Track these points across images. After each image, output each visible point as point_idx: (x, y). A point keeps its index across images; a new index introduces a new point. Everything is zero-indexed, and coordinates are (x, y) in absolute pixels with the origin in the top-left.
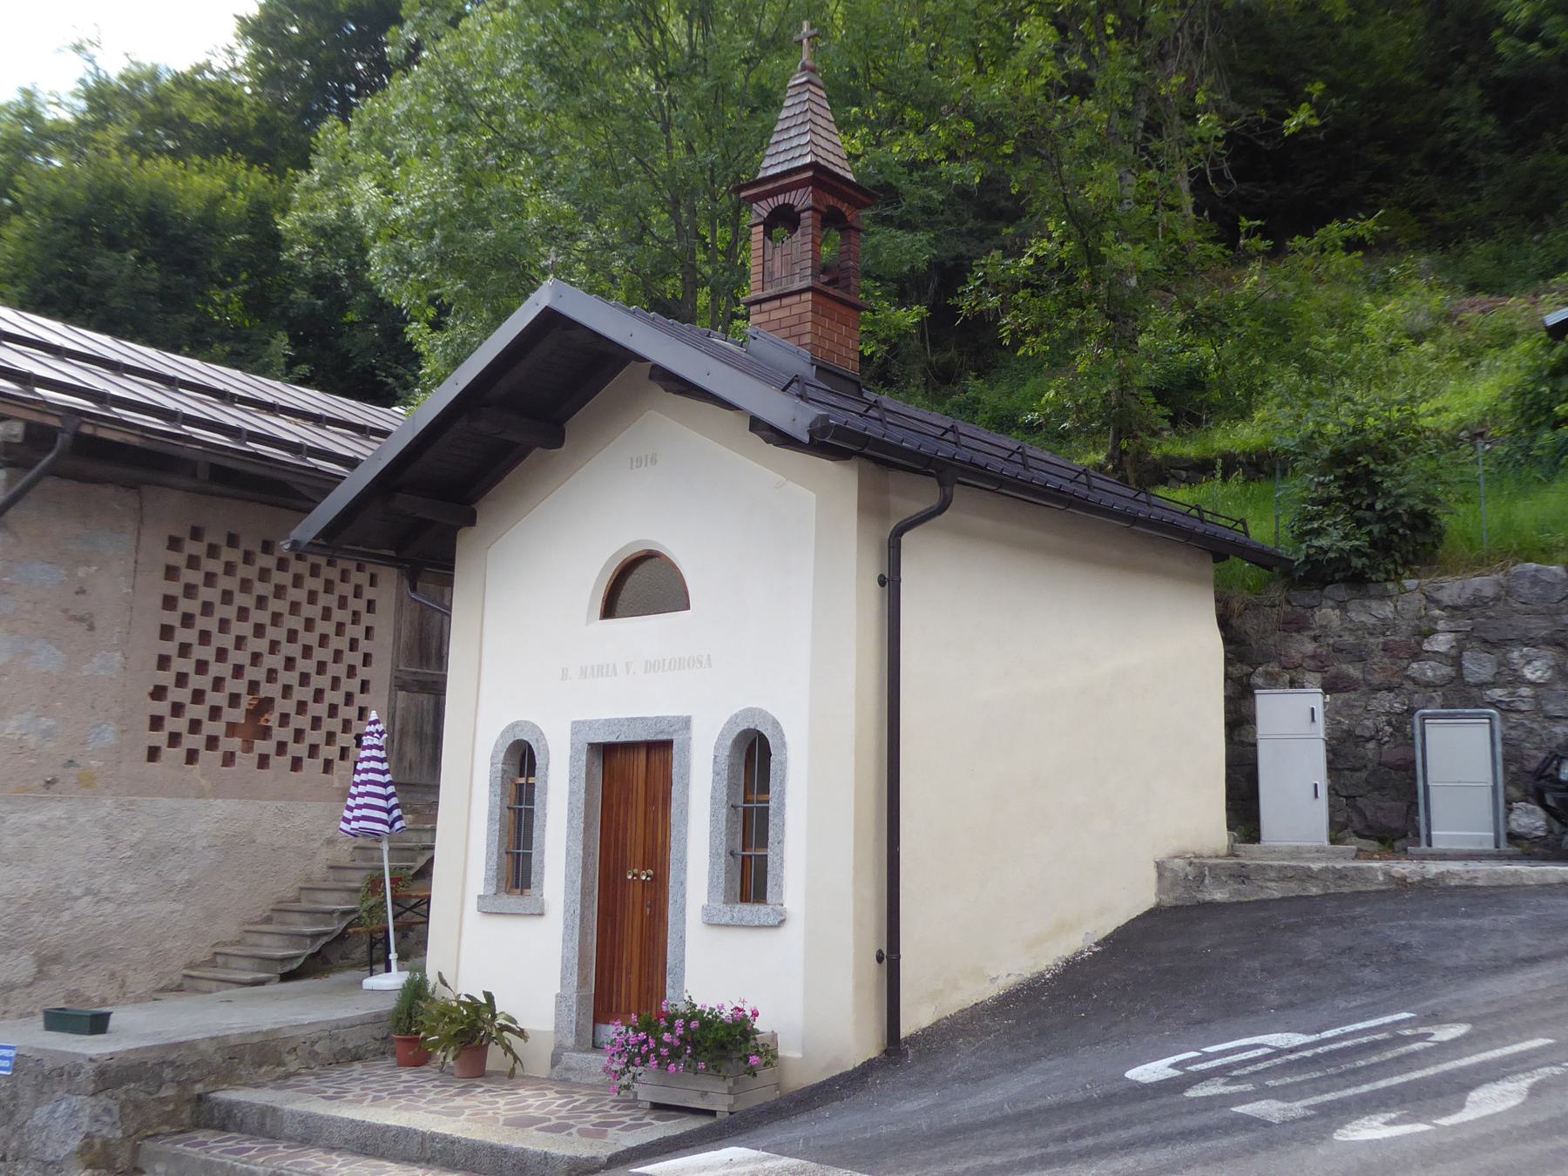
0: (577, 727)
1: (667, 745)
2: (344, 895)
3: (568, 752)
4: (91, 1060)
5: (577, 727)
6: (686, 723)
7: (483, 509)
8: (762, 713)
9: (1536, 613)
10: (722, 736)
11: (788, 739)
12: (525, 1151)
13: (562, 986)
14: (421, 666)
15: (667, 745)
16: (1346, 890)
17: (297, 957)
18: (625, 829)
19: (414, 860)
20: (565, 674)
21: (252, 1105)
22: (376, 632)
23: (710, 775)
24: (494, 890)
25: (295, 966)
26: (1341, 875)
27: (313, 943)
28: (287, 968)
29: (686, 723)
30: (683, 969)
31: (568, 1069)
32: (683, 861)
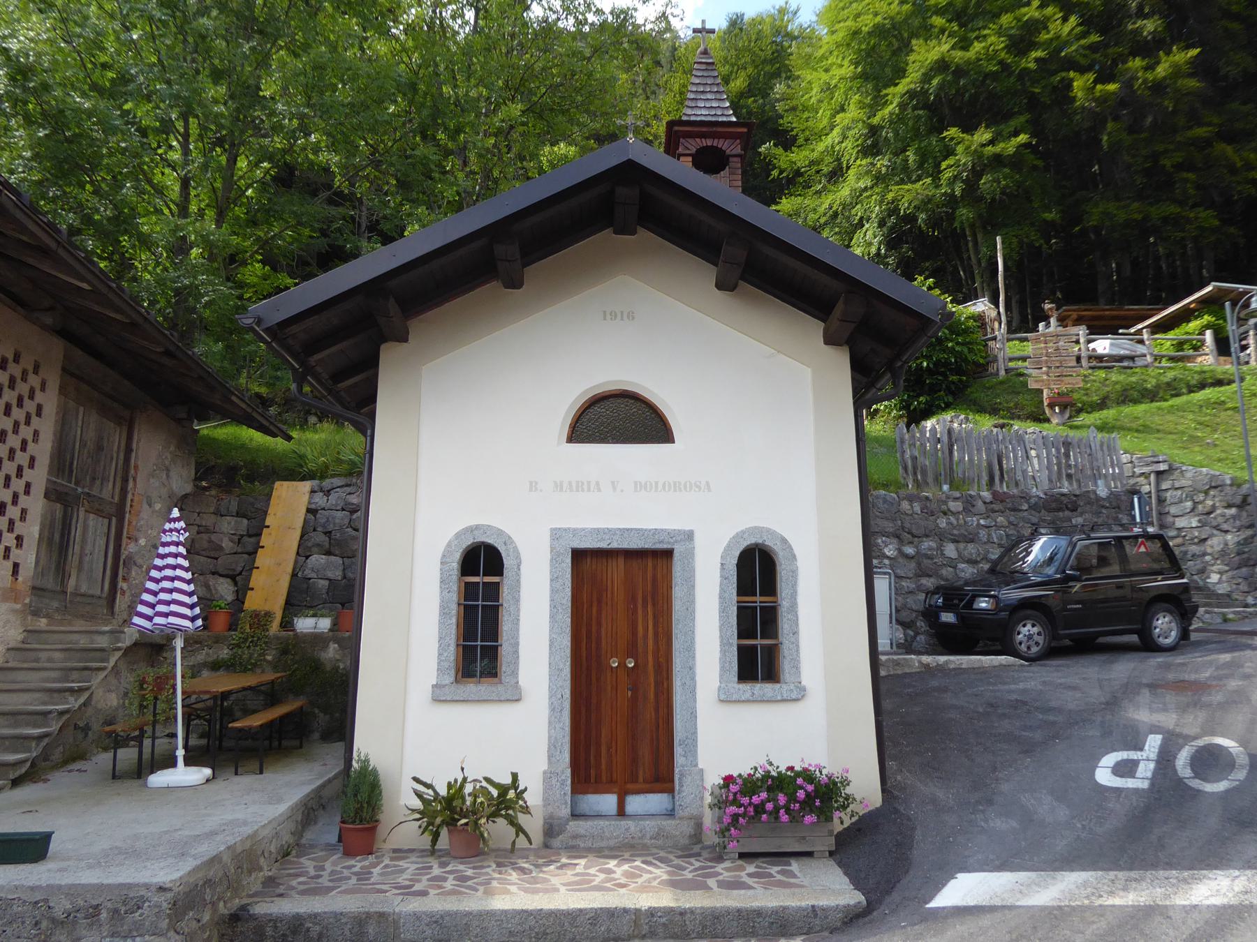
0: (556, 534)
1: (668, 554)
2: (37, 695)
3: (546, 556)
4: (162, 889)
5: (556, 534)
6: (690, 536)
7: (416, 327)
8: (508, 540)
9: (887, 519)
10: (728, 548)
11: (797, 551)
12: (785, 908)
13: (550, 762)
14: (57, 477)
15: (668, 554)
16: (900, 672)
17: (24, 761)
18: (599, 624)
19: (107, 660)
20: (533, 486)
21: (337, 916)
22: (42, 436)
23: (717, 579)
24: (452, 679)
25: (23, 770)
26: (897, 663)
27: (38, 745)
28: (17, 774)
29: (690, 536)
30: (695, 741)
31: (575, 837)
32: (690, 649)
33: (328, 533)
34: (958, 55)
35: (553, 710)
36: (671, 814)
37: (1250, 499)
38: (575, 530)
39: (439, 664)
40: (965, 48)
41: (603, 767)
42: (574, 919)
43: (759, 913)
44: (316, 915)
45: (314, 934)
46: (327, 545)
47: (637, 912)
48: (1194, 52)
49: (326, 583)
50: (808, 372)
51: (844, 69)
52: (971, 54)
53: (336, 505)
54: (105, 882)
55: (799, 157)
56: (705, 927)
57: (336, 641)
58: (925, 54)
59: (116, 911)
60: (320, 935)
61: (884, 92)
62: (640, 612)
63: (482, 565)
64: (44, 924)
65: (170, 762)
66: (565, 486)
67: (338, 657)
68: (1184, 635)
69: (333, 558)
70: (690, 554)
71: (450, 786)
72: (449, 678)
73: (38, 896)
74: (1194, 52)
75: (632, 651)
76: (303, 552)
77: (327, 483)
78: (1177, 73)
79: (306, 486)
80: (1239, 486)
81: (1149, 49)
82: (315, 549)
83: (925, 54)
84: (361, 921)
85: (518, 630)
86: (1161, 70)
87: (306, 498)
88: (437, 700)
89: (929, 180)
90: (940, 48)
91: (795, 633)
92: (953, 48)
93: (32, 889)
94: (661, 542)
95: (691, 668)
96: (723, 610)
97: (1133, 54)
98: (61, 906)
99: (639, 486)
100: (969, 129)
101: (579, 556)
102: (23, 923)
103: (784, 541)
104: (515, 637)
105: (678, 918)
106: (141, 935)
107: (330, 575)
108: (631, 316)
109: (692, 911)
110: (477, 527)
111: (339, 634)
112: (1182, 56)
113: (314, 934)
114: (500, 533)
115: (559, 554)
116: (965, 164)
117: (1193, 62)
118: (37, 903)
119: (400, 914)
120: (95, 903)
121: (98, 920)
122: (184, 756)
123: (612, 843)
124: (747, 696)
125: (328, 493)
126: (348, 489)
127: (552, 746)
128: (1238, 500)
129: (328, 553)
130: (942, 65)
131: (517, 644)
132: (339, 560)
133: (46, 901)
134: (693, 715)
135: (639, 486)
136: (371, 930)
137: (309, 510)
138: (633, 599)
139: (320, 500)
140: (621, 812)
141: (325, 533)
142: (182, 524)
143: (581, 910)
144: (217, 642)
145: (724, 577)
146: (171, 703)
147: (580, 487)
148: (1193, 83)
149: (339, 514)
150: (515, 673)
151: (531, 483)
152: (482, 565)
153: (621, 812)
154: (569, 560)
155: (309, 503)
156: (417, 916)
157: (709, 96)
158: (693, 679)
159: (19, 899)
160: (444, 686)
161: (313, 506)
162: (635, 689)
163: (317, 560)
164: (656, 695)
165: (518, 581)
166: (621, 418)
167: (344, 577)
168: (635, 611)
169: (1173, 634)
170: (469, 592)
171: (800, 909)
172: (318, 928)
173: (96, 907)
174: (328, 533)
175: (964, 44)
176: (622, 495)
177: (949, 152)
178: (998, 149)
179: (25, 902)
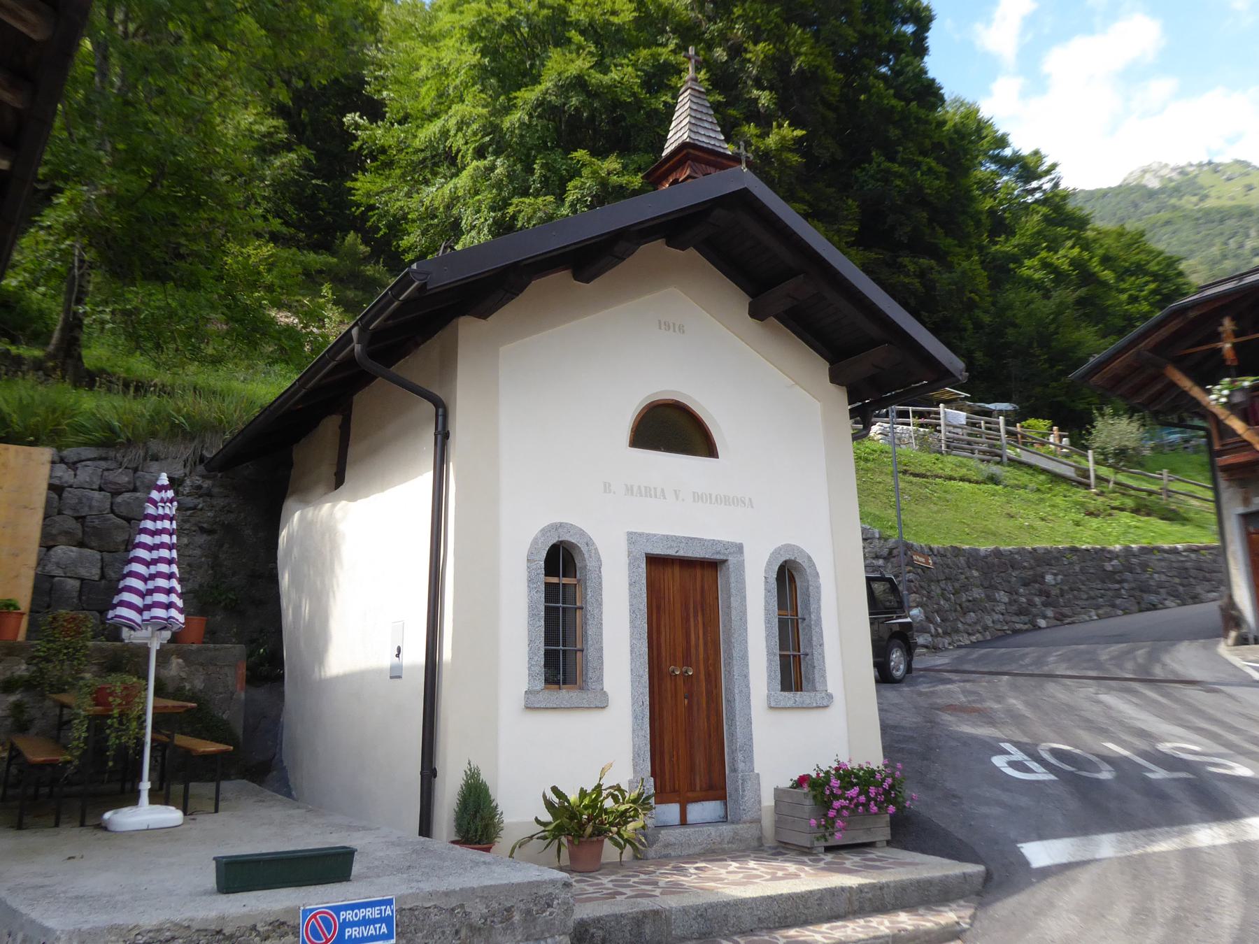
0: (633, 538)
3: (624, 560)
5: (633, 538)
6: (740, 548)
8: (589, 543)
12: (947, 877)
13: (635, 771)
20: (607, 488)
21: (618, 918)
30: (751, 746)
31: (667, 846)
32: (744, 657)
33: (80, 519)
34: (596, 77)
35: (635, 718)
36: (724, 819)
37: (895, 552)
38: (648, 535)
39: (529, 669)
40: (606, 71)
41: (667, 776)
42: (806, 901)
43: (930, 882)
44: (599, 920)
45: (598, 940)
46: (80, 534)
47: (851, 888)
48: (799, 133)
49: (77, 583)
50: (818, 405)
51: (461, 57)
52: (606, 79)
53: (92, 482)
54: (515, 881)
55: (380, 134)
56: (896, 898)
57: (180, 655)
58: (562, 65)
59: (529, 912)
60: (604, 940)
61: (515, 94)
62: (692, 620)
63: (561, 561)
64: (463, 933)
65: (131, 798)
66: (635, 489)
67: (183, 675)
68: (909, 669)
69: (87, 551)
70: (741, 566)
71: (583, 794)
72: (540, 684)
73: (454, 902)
74: (799, 133)
75: (687, 661)
76: (48, 543)
77: (70, 453)
78: (783, 147)
79: (44, 454)
80: (886, 540)
81: (764, 121)
82: (62, 539)
83: (562, 65)
84: (639, 920)
85: (601, 634)
86: (772, 141)
87: (46, 469)
88: (529, 708)
89: (550, 198)
90: (580, 64)
91: (822, 645)
92: (591, 67)
93: (447, 894)
94: (718, 553)
95: (746, 676)
96: (768, 621)
97: (748, 120)
98: (477, 910)
99: (697, 497)
100: (601, 154)
101: (656, 563)
102: (443, 933)
103: (809, 558)
104: (599, 640)
105: (879, 892)
106: (552, 936)
107: (83, 572)
108: (682, 329)
109: (887, 885)
110: (561, 525)
111: (186, 647)
112: (789, 132)
113: (598, 940)
114: (582, 533)
115: (635, 559)
116: (589, 188)
117: (798, 141)
118: (453, 910)
119: (670, 911)
120: (508, 905)
121: (512, 924)
122: (151, 791)
123: (697, 849)
124: (790, 703)
125: (73, 466)
126: (103, 464)
127: (636, 755)
128: (885, 552)
129: (81, 544)
130: (579, 83)
131: (601, 649)
132: (98, 556)
133: (462, 906)
134: (749, 722)
135: (697, 497)
136: (648, 929)
137: (51, 487)
138: (687, 608)
139: (61, 470)
140: (684, 822)
141: (77, 518)
142: (170, 494)
143: (811, 892)
144: (8, 655)
145: (768, 591)
146: (141, 719)
147: (648, 492)
148: (795, 159)
149: (96, 495)
150: (600, 679)
151: (605, 484)
152: (561, 561)
153: (684, 822)
154: (644, 565)
155: (51, 477)
156: (685, 911)
157: (706, 125)
158: (748, 686)
159: (435, 907)
160: (538, 692)
161: (57, 482)
162: (689, 696)
163: (64, 552)
164: (707, 703)
165: (600, 583)
166: (671, 428)
167: (103, 576)
168: (688, 620)
169: (902, 667)
170: (551, 592)
171: (957, 876)
172: (601, 933)
173: (509, 910)
174: (80, 519)
175: (602, 67)
176: (678, 503)
177: (575, 173)
178: (624, 180)
179: (442, 909)
